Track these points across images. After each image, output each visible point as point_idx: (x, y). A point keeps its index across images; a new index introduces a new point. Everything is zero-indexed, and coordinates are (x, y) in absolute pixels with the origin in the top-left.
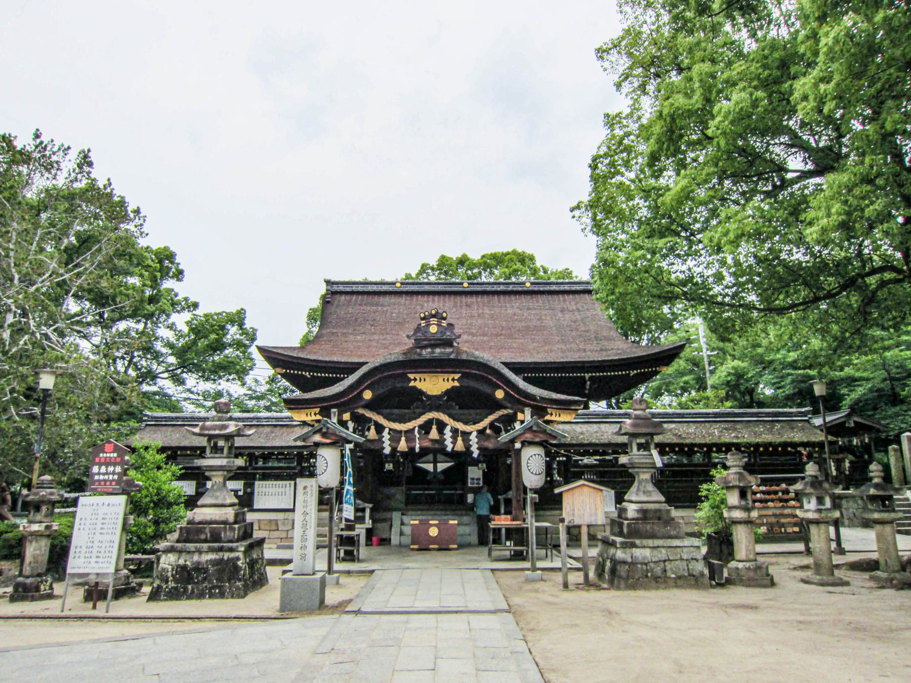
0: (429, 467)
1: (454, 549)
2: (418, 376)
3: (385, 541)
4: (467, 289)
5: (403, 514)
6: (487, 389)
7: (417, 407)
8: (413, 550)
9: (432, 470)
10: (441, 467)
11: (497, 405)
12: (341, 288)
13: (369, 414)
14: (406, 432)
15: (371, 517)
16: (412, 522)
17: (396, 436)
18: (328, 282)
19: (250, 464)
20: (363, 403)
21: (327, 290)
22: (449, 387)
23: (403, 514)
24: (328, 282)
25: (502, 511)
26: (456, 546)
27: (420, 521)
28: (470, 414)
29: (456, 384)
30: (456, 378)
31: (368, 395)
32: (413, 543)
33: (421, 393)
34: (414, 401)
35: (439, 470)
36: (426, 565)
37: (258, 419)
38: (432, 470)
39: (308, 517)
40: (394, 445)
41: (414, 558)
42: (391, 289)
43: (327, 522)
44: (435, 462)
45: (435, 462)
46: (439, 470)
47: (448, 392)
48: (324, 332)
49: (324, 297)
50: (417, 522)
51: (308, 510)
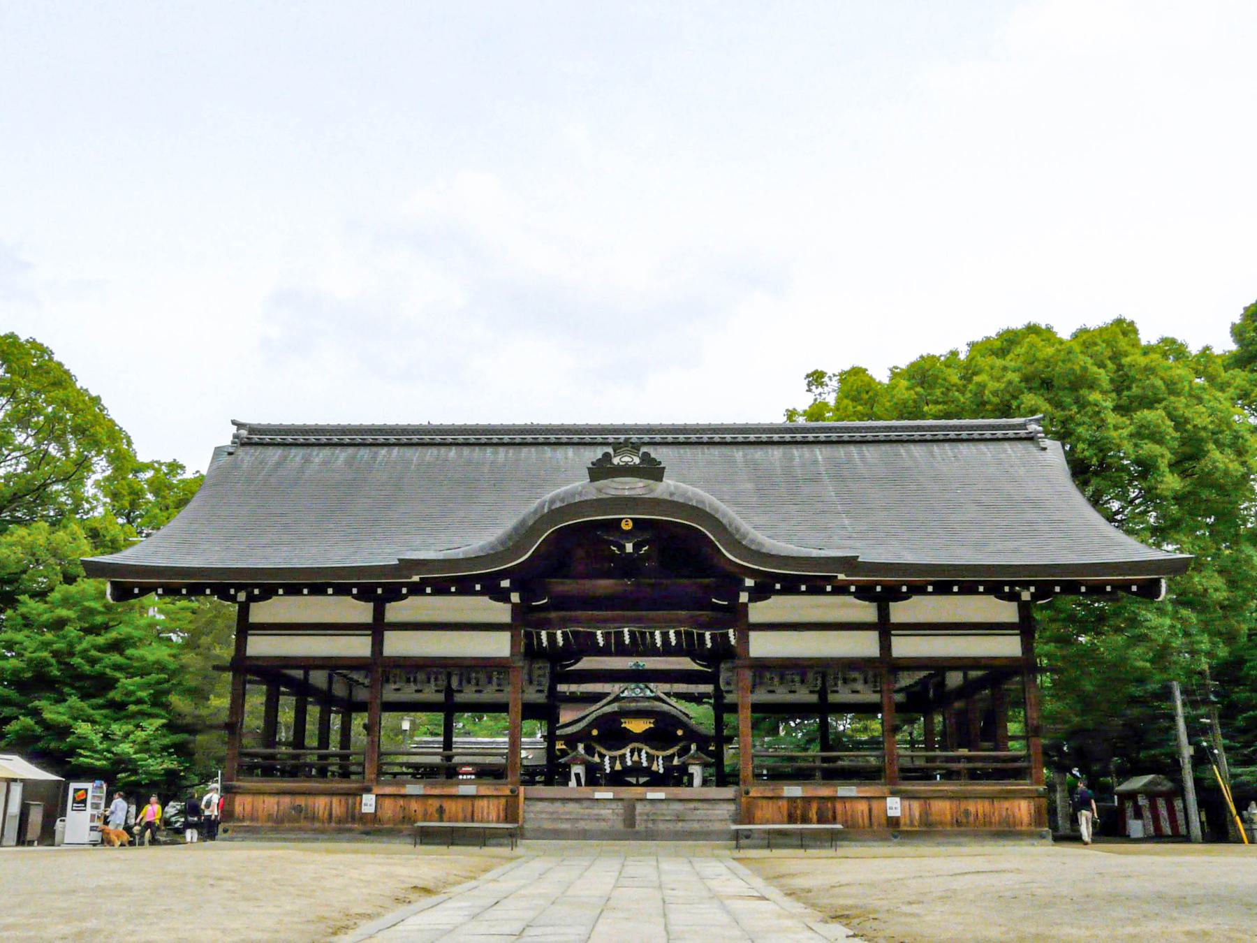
11: (677, 740)
17: (613, 759)
34: (625, 738)
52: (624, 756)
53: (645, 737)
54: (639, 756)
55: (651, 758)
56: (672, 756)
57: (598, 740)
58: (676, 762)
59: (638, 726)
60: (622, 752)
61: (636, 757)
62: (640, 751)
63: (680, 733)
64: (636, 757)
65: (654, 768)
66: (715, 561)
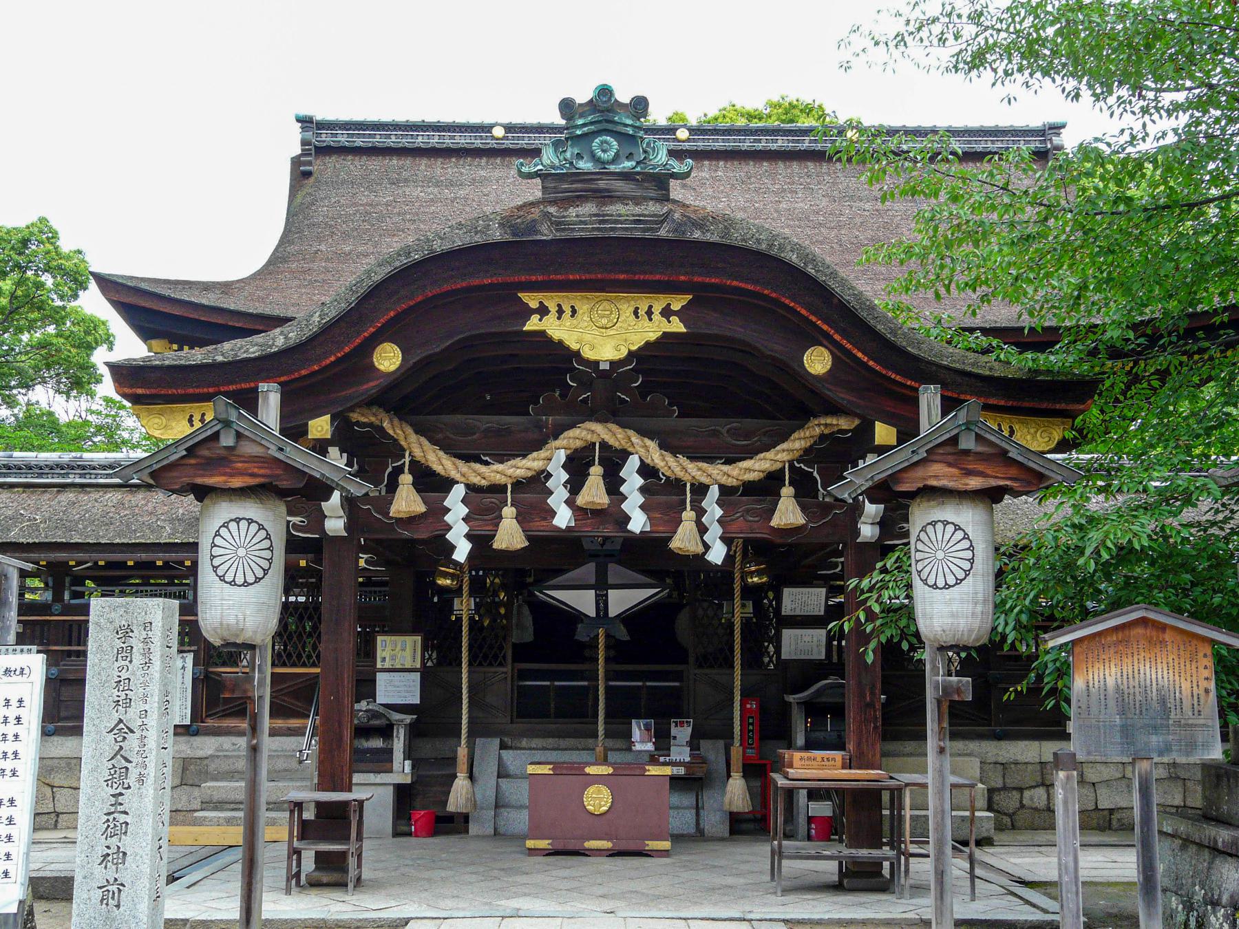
0: (584, 601)
1: (664, 853)
2: (551, 302)
3: (450, 824)
4: (686, 146)
5: (503, 746)
6: (772, 344)
7: (548, 411)
8: (533, 852)
9: (592, 613)
10: (621, 601)
11: (801, 401)
12: (343, 139)
13: (393, 428)
14: (518, 485)
15: (408, 755)
16: (531, 769)
17: (484, 502)
18: (306, 122)
19: (58, 597)
20: (371, 386)
21: (304, 143)
22: (653, 337)
23: (503, 746)
24: (306, 122)
25: (800, 740)
26: (666, 845)
27: (556, 766)
28: (715, 433)
29: (677, 326)
30: (676, 307)
31: (388, 359)
32: (535, 833)
33: (561, 359)
34: (546, 385)
35: (613, 611)
36: (578, 906)
37: (85, 468)
38: (592, 613)
39: (133, 742)
40: (484, 530)
41: (539, 878)
42: (478, 143)
43: (242, 764)
44: (601, 586)
45: (601, 586)
46: (613, 611)
47: (646, 358)
48: (291, 249)
49: (296, 162)
50: (546, 770)
51: (132, 717)
52: (539, 480)
53: (660, 388)
54: (613, 483)
55: (665, 494)
56: (768, 487)
57: (409, 398)
58: (788, 512)
59: (604, 331)
60: (521, 467)
61: (594, 492)
62: (613, 461)
63: (817, 362)
64: (594, 492)
65: (684, 540)
66: (283, 509)
